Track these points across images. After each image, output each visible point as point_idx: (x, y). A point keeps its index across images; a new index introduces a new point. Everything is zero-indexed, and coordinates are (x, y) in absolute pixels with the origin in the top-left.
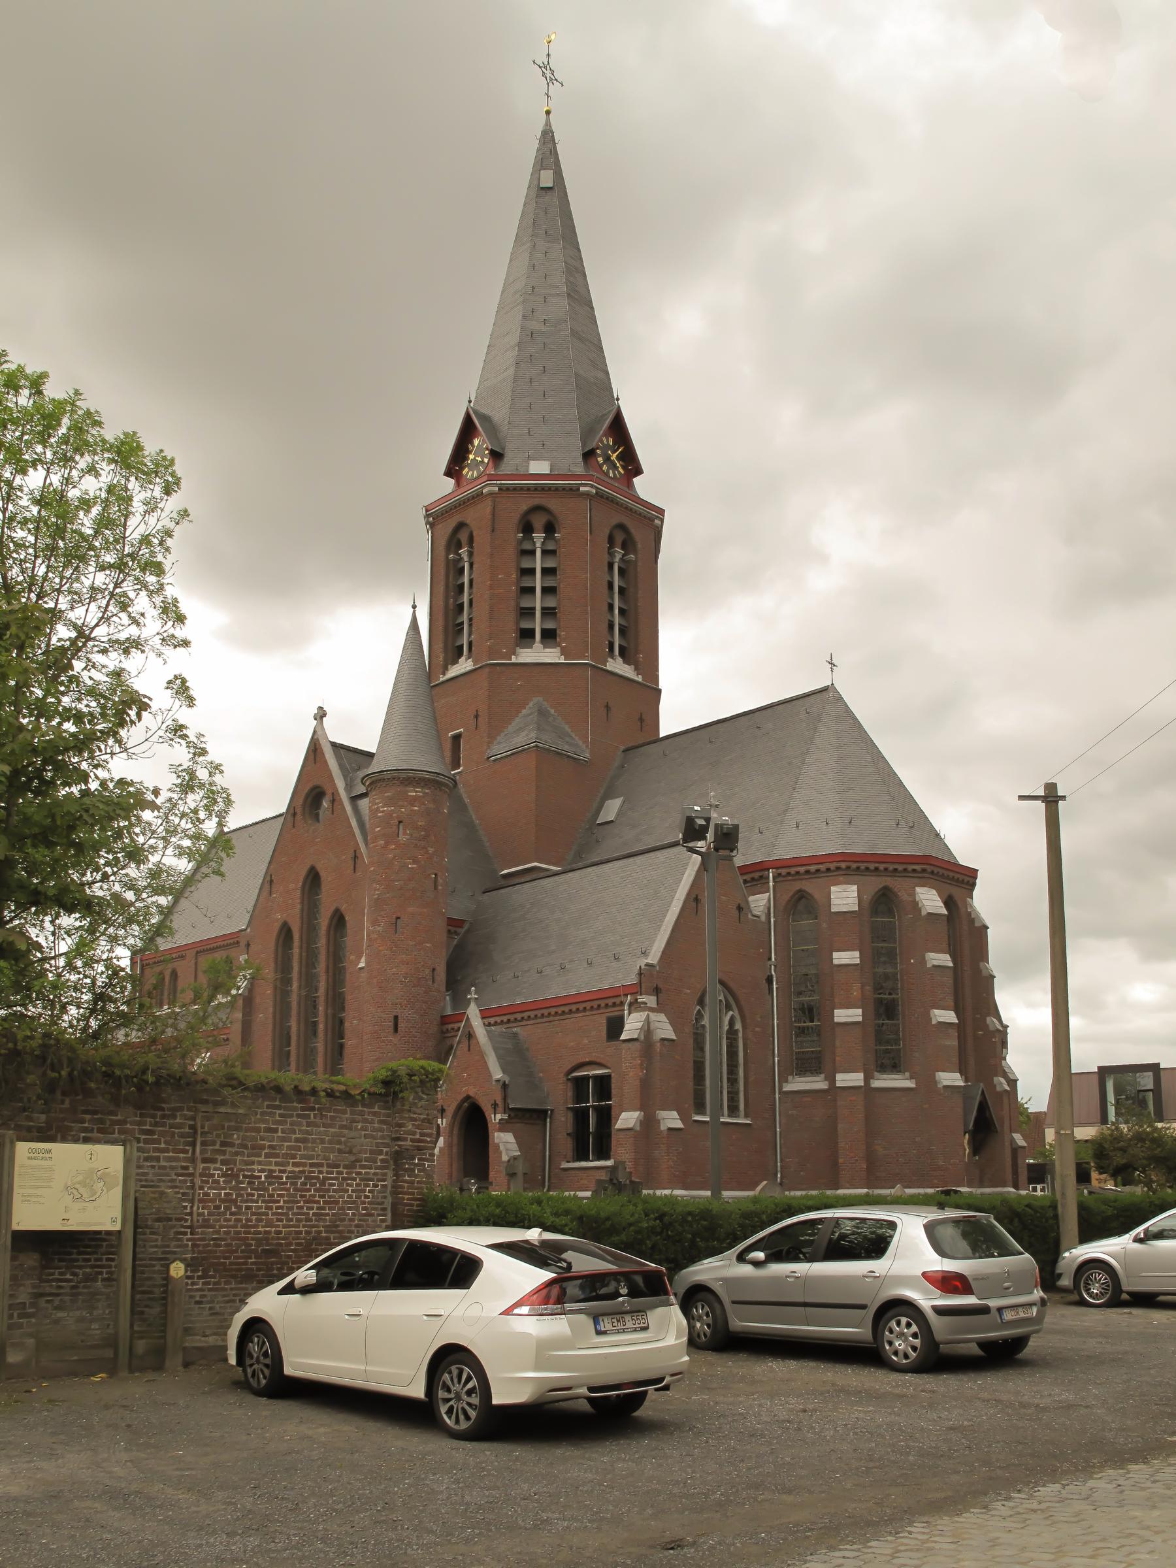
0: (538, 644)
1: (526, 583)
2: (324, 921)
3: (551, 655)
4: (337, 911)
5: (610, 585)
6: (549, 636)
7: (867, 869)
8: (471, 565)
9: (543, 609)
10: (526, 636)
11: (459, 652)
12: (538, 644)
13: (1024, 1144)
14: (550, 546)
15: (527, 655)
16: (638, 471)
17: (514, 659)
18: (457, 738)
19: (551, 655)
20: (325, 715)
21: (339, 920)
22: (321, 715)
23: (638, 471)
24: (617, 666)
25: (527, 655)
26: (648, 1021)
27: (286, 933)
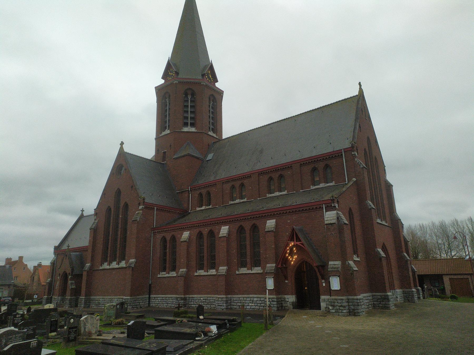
0: (189, 127)
1: (186, 115)
2: (122, 205)
3: (193, 130)
4: (126, 202)
5: (209, 116)
6: (192, 125)
7: (335, 156)
8: (169, 104)
9: (190, 106)
10: (186, 124)
11: (166, 128)
12: (189, 127)
13: (356, 269)
14: (193, 100)
15: (186, 129)
16: (217, 81)
17: (182, 131)
18: (164, 153)
19: (193, 130)
20: (123, 144)
21: (126, 205)
22: (122, 144)
23: (217, 81)
24: (211, 133)
25: (186, 129)
26: (337, 214)
27: (109, 210)
